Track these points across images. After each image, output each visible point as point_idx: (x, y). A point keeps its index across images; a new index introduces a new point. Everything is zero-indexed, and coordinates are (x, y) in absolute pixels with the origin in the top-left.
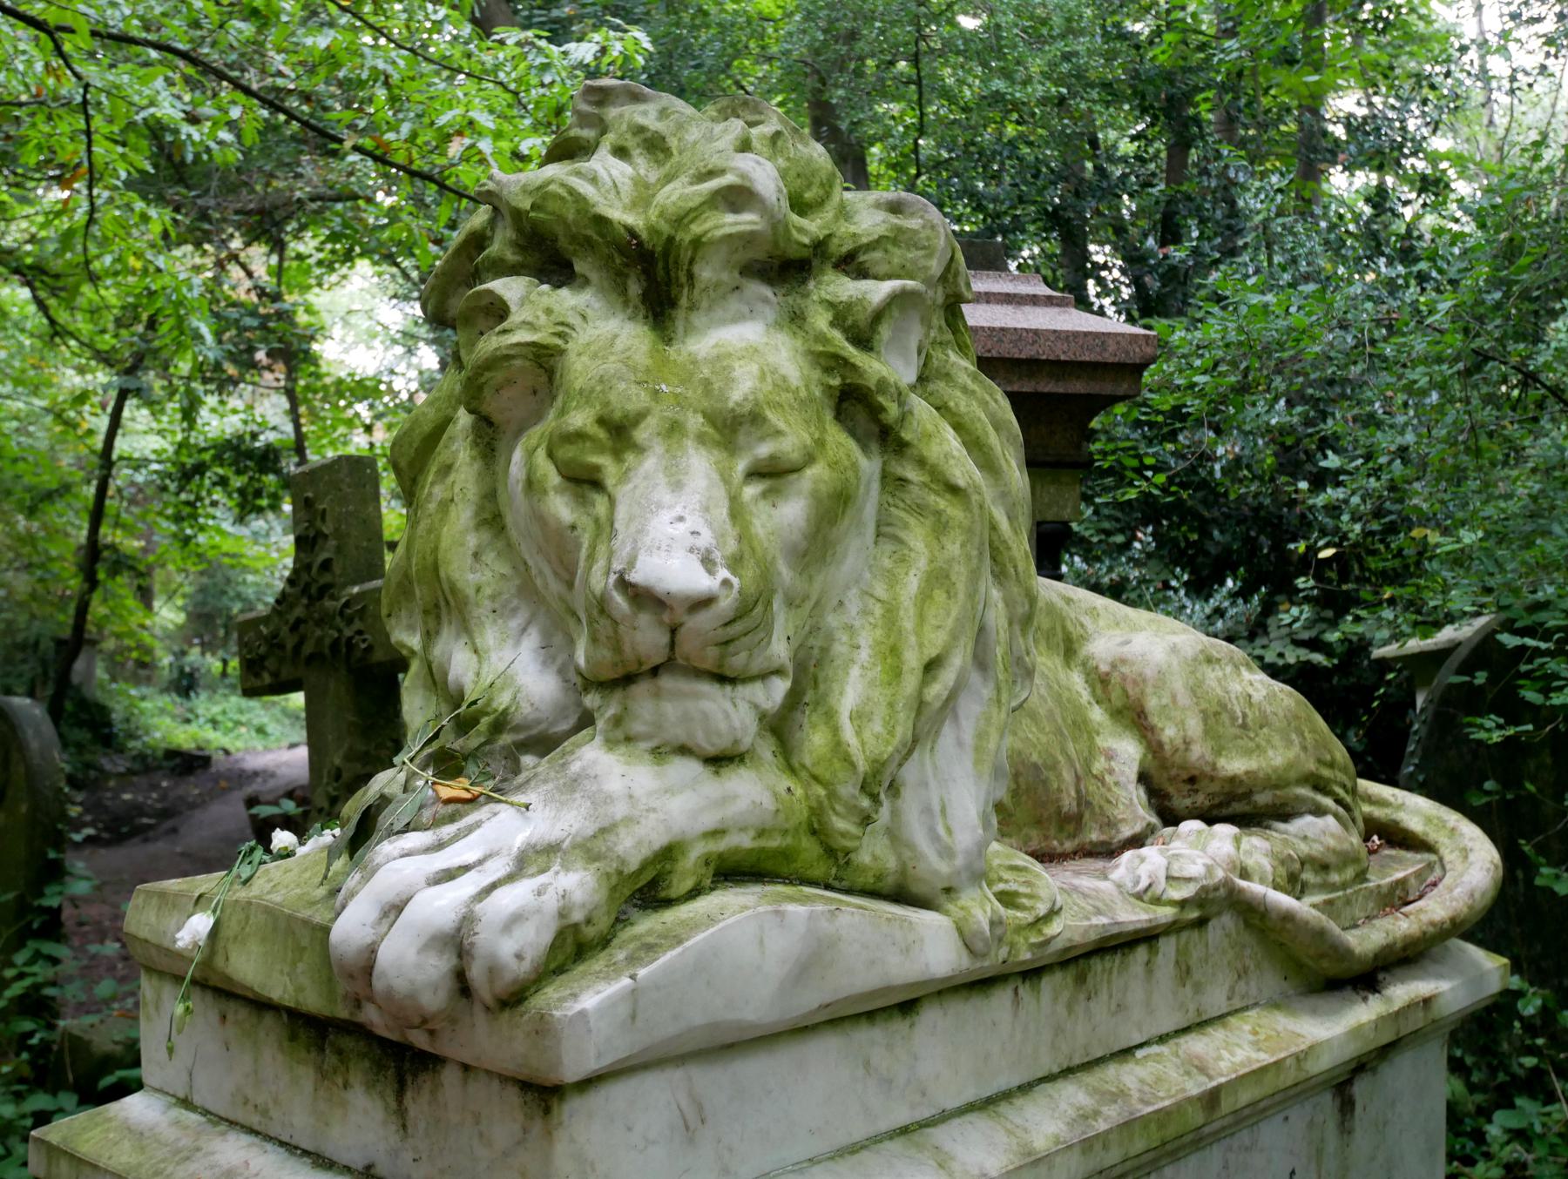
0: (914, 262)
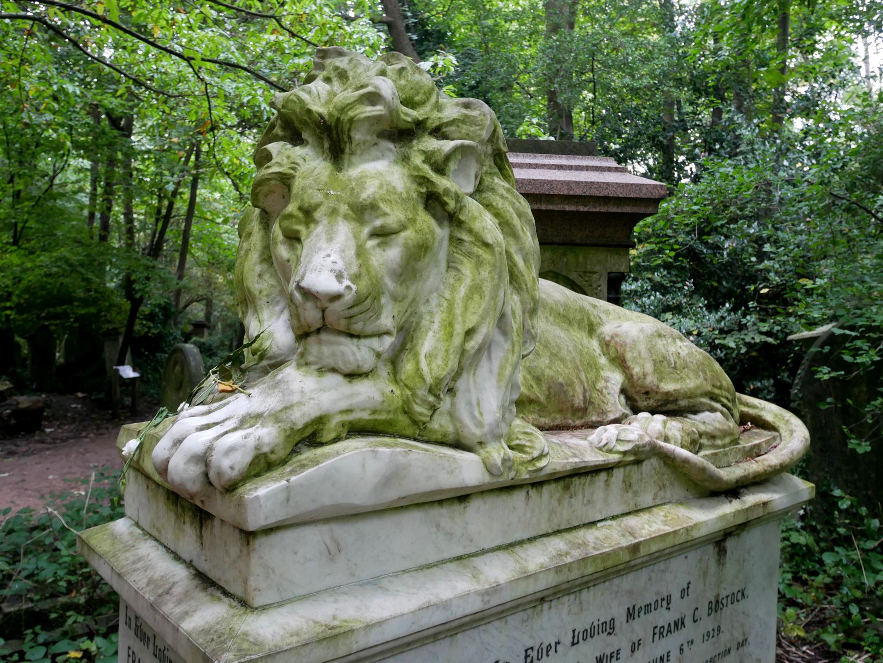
0: (474, 132)
